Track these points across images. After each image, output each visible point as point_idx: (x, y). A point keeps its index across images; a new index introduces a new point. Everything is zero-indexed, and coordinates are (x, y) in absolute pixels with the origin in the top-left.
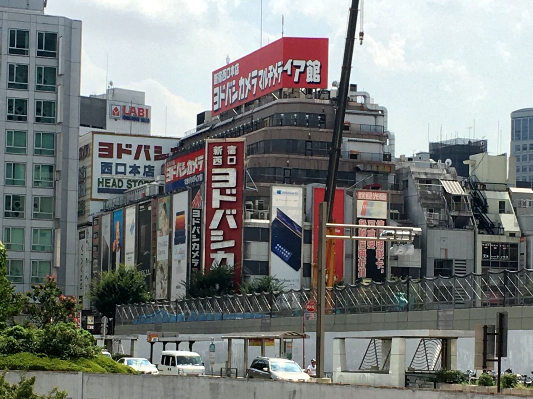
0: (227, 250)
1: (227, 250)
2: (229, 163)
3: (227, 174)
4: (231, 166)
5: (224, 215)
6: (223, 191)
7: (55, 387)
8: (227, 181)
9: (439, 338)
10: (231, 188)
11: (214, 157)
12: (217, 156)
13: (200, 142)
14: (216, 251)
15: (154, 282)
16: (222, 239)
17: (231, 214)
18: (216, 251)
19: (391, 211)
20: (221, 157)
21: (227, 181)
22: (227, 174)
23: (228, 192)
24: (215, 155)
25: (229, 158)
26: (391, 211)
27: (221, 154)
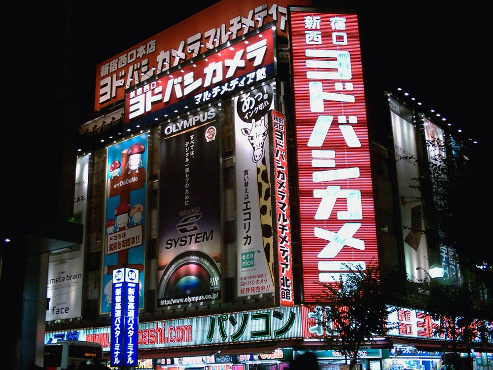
0: (344, 184)
1: (344, 184)
2: (334, 42)
3: (335, 59)
4: (342, 48)
5: (335, 123)
6: (329, 85)
7: (64, 271)
8: (336, 70)
9: (319, 80)
10: (344, 82)
11: (306, 32)
12: (311, 30)
13: (423, 118)
14: (324, 185)
15: (229, 193)
16: (334, 165)
17: (348, 123)
18: (324, 185)
19: (294, 242)
20: (320, 33)
21: (336, 70)
22: (335, 59)
23: (338, 86)
24: (307, 29)
25: (334, 35)
26: (294, 242)
27: (318, 27)
